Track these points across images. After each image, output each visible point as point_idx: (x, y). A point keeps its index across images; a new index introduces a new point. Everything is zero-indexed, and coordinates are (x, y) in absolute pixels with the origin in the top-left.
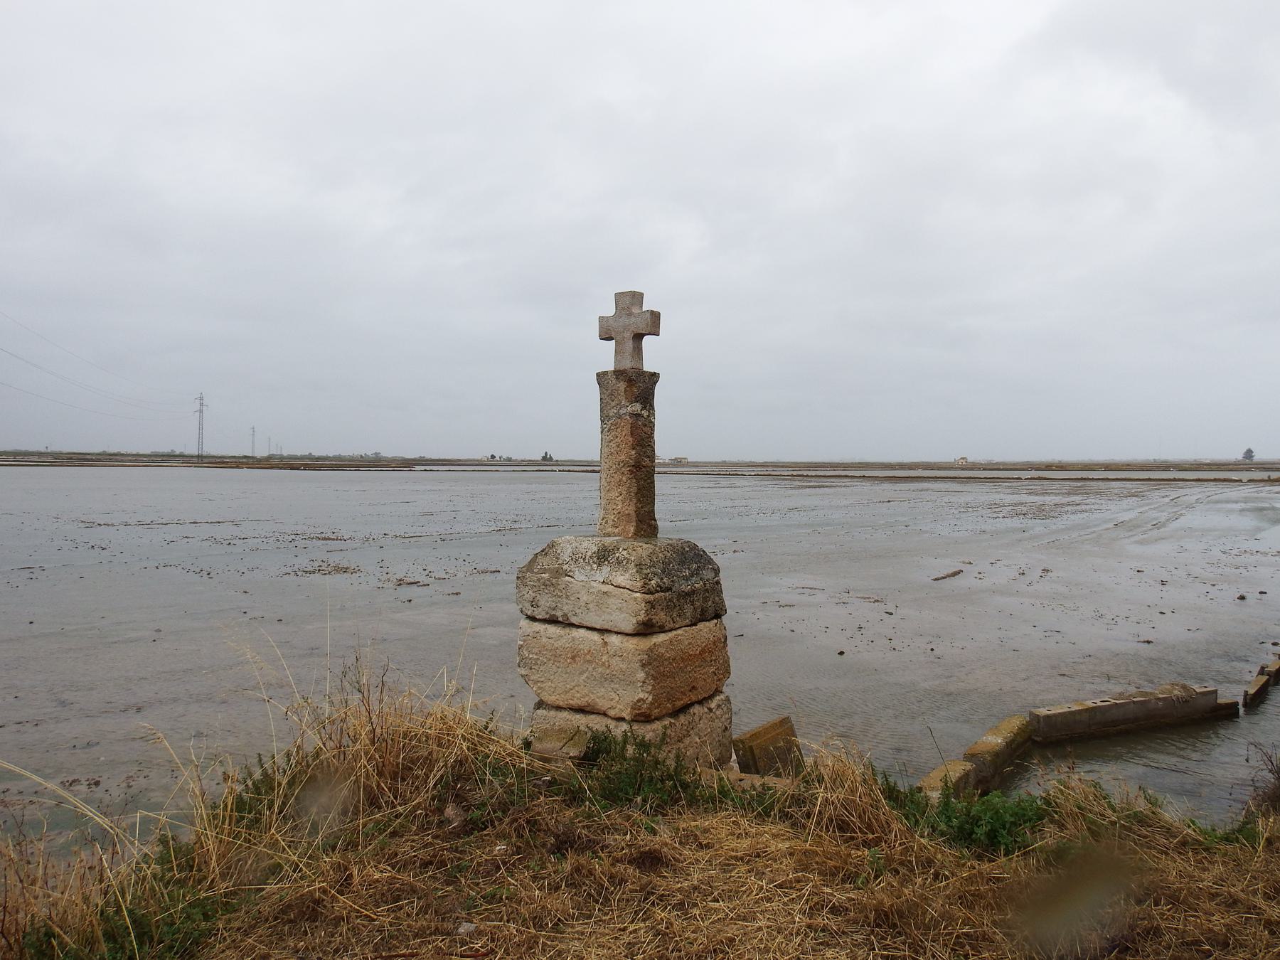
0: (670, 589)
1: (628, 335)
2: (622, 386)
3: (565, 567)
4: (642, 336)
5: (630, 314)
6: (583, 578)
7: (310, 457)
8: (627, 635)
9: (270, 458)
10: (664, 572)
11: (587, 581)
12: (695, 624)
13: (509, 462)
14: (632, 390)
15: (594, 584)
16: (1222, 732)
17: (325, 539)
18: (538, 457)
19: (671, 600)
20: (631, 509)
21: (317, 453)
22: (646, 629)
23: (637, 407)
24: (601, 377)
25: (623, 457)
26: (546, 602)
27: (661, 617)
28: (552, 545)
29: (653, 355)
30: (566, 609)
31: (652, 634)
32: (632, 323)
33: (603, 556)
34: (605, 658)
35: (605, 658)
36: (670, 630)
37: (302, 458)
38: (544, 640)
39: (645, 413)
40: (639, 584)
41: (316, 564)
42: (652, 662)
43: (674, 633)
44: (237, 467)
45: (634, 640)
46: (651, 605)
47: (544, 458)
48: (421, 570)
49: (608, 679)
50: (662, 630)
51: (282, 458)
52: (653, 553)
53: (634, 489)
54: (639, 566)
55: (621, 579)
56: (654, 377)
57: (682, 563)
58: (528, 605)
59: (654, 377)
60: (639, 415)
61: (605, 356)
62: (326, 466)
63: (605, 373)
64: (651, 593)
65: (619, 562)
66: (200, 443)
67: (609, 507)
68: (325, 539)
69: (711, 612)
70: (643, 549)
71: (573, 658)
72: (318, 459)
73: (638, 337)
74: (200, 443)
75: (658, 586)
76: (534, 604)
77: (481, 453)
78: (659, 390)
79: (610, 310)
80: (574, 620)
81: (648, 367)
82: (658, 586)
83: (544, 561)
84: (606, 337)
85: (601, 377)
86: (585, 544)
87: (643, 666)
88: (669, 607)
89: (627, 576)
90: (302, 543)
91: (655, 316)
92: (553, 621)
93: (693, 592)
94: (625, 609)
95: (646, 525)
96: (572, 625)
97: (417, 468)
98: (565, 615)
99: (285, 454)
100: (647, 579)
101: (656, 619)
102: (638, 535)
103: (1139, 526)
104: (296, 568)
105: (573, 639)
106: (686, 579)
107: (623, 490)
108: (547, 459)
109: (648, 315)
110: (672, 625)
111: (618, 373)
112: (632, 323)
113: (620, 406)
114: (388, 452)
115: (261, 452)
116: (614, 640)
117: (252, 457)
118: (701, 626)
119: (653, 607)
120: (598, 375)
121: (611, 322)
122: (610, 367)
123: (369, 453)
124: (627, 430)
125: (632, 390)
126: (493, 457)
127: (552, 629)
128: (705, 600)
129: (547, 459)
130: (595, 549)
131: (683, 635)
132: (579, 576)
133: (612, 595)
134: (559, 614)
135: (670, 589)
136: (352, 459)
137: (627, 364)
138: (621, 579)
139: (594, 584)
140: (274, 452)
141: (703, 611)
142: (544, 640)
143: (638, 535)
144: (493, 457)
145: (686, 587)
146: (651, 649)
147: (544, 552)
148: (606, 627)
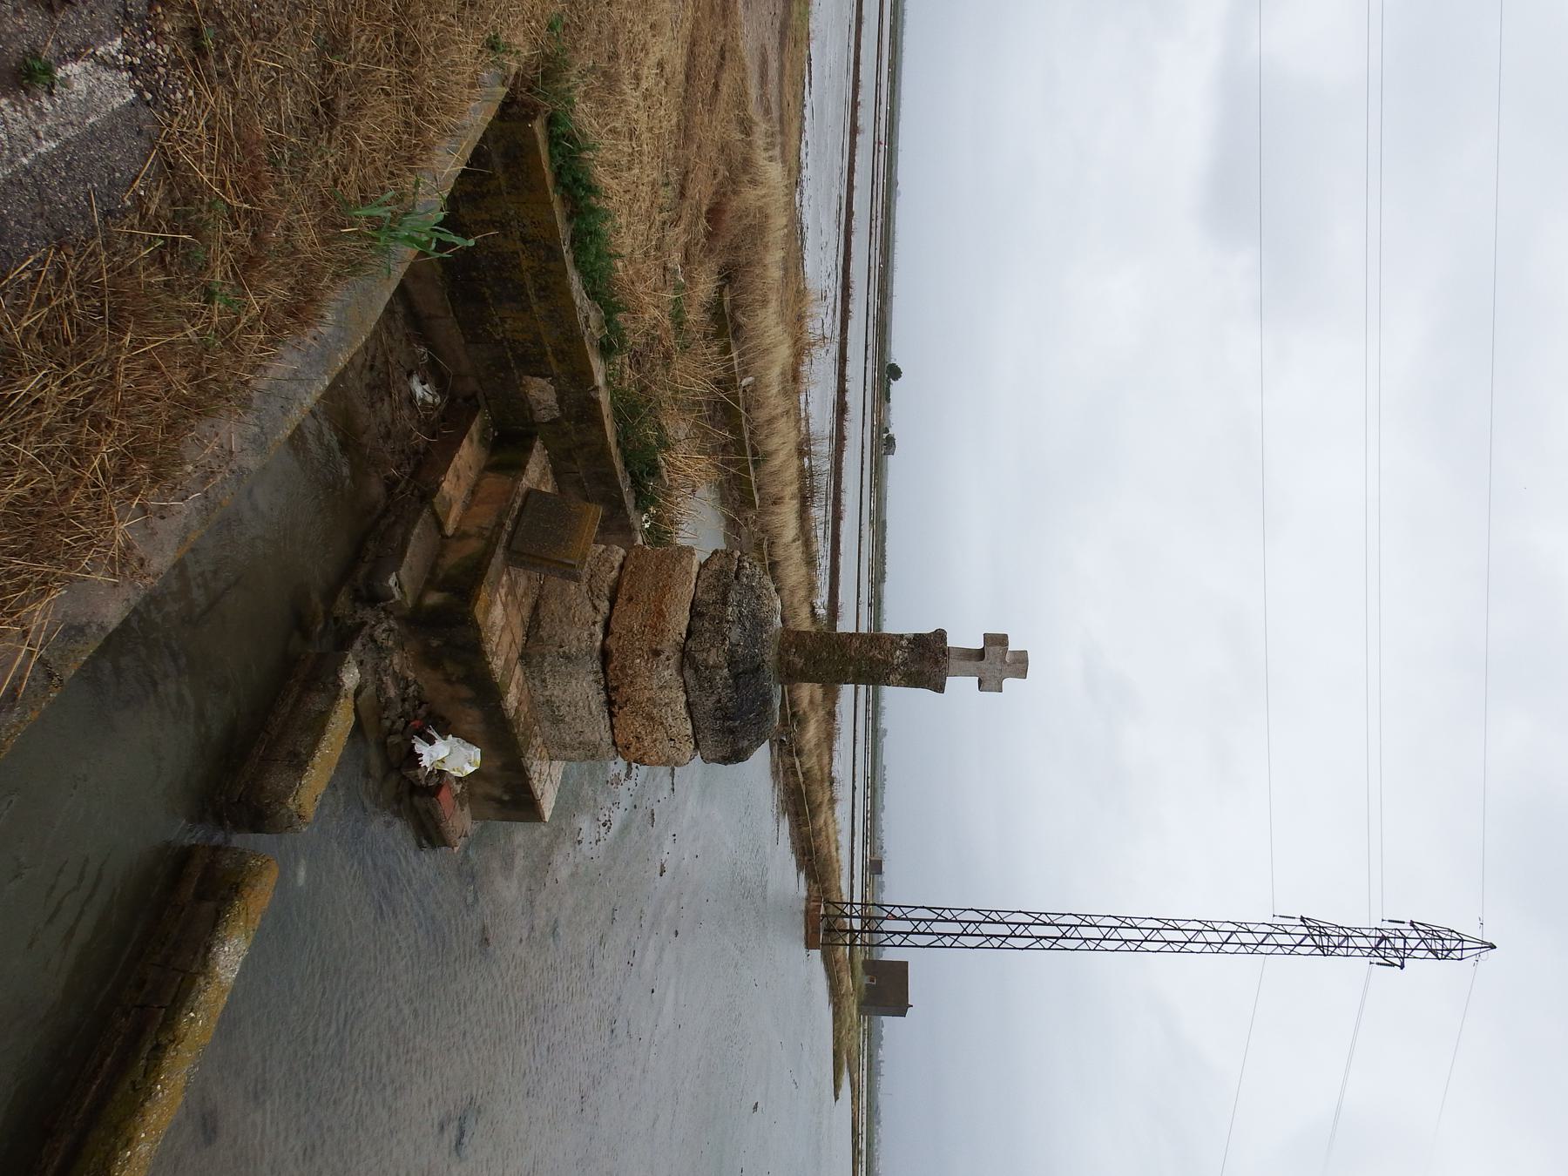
0: (737, 577)
14: (926, 660)
24: (941, 635)
29: (961, 686)
32: (997, 661)
39: (904, 643)
43: (694, 576)
56: (940, 688)
59: (940, 688)
77: (886, 722)
78: (925, 694)
79: (1008, 683)
81: (950, 682)
85: (941, 635)
93: (725, 603)
103: (782, 45)
106: (739, 605)
112: (997, 661)
114: (889, 589)
125: (926, 660)
131: (686, 591)
135: (737, 577)
141: (701, 615)
145: (732, 597)
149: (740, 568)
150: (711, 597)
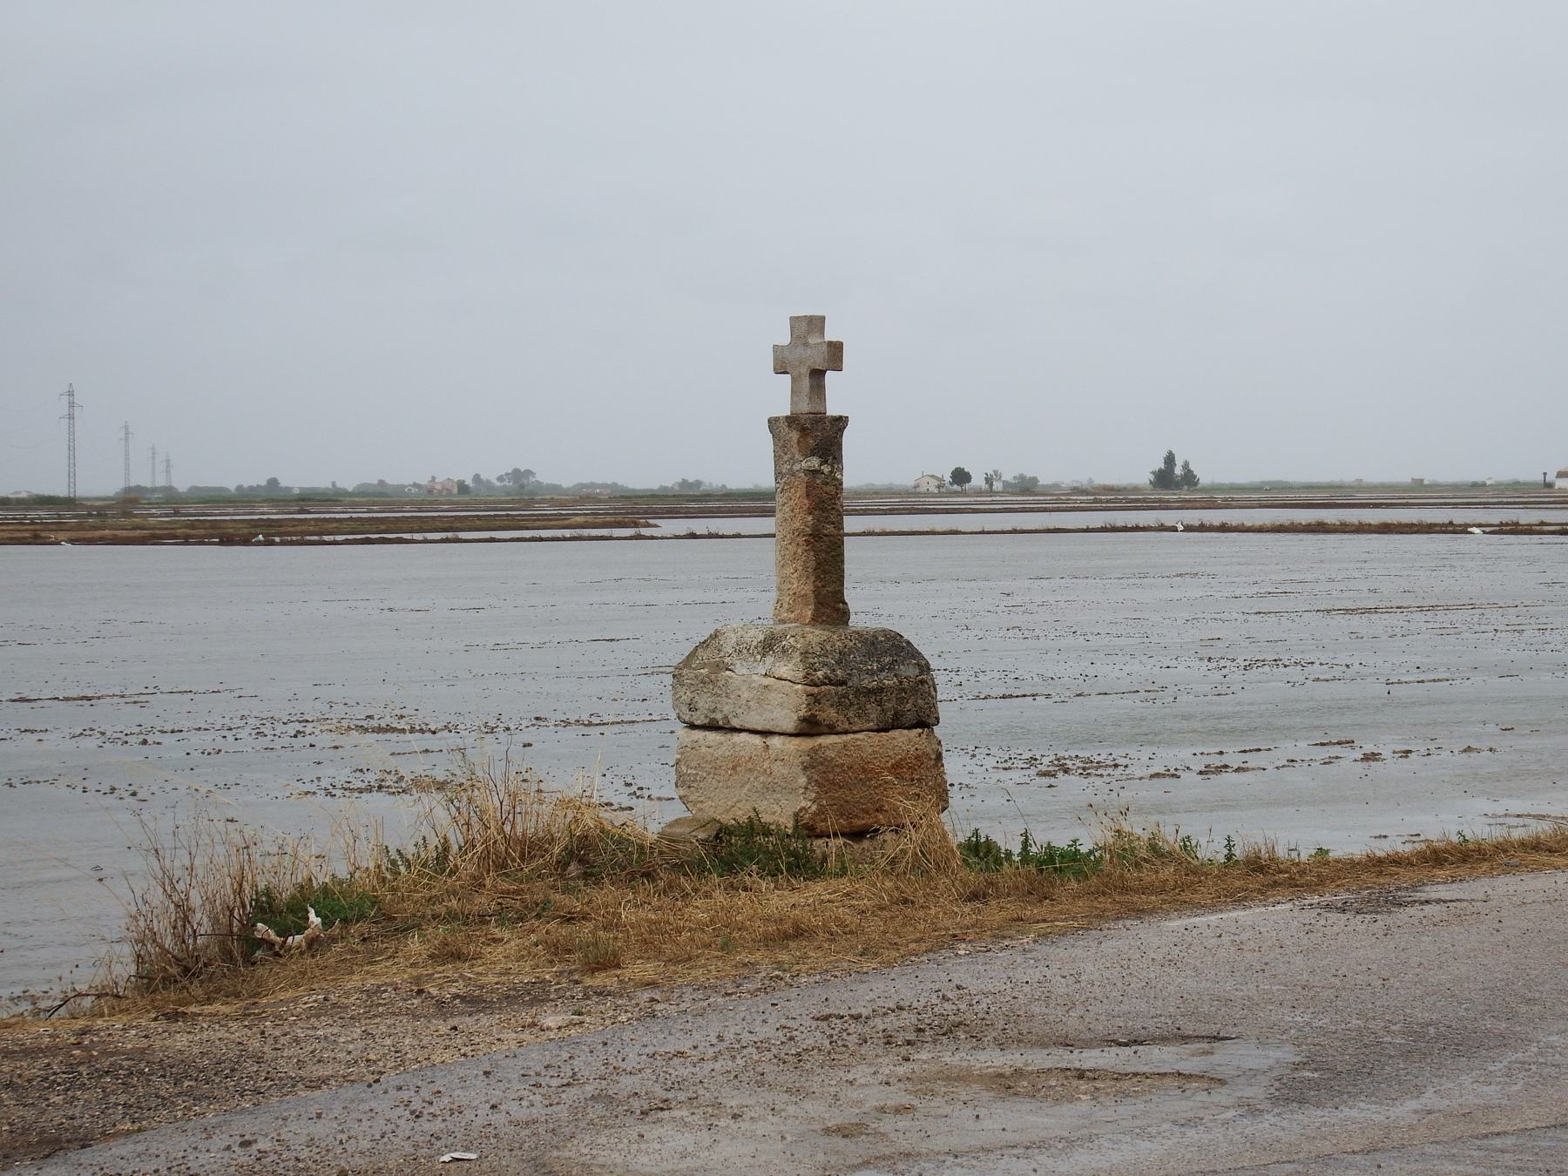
0: (843, 683)
1: (805, 371)
2: (795, 436)
3: (727, 660)
4: (822, 373)
5: (806, 344)
6: (744, 671)
7: (274, 494)
8: (791, 735)
9: (130, 501)
10: (839, 662)
11: (747, 674)
12: (886, 730)
13: (1027, 494)
14: (815, 436)
15: (755, 677)
16: (1455, 839)
17: (379, 730)
18: (1139, 474)
19: (845, 696)
20: (808, 589)
21: (299, 477)
22: (810, 727)
23: (814, 462)
24: (773, 422)
25: (797, 525)
26: (704, 702)
27: (829, 714)
28: (714, 636)
30: (726, 709)
31: (819, 734)
32: (812, 357)
33: (769, 645)
34: (766, 765)
35: (766, 765)
36: (846, 732)
37: (245, 498)
38: (704, 749)
39: (826, 469)
40: (801, 675)
41: (371, 778)
42: (813, 763)
43: (844, 738)
44: (36, 539)
45: (797, 741)
46: (815, 699)
47: (1164, 478)
48: (619, 784)
49: (769, 788)
50: (832, 730)
51: (172, 500)
52: (828, 640)
53: (812, 564)
54: (805, 654)
55: (784, 670)
56: (840, 422)
57: (870, 655)
58: (685, 709)
59: (840, 422)
60: (815, 473)
61: (780, 397)
62: (338, 527)
63: (777, 419)
64: (816, 685)
65: (784, 651)
66: (72, 475)
67: (784, 587)
68: (379, 730)
69: (910, 717)
70: (816, 635)
71: (734, 768)
72: (306, 500)
73: (817, 375)
74: (72, 475)
75: (826, 677)
76: (692, 708)
78: (850, 441)
79: (785, 338)
80: (735, 723)
81: (832, 410)
82: (826, 677)
83: (704, 655)
84: (780, 369)
85: (773, 422)
86: (751, 633)
87: (805, 769)
88: (841, 704)
89: (790, 666)
90: (325, 740)
91: (836, 350)
92: (712, 727)
93: (881, 690)
94: (785, 710)
95: (829, 604)
96: (734, 730)
97: (668, 526)
98: (726, 717)
99: (182, 484)
100: (812, 668)
101: (821, 716)
102: (816, 620)
104: (325, 783)
105: (734, 745)
106: (872, 673)
107: (799, 565)
108: (1172, 481)
109: (825, 348)
110: (847, 726)
111: (792, 420)
112: (812, 357)
113: (793, 461)
114: (564, 467)
115: (99, 481)
116: (776, 741)
117: (69, 503)
118: (895, 733)
119: (817, 701)
120: (770, 421)
121: (786, 353)
122: (786, 411)
123: (491, 474)
124: (801, 491)
126: (961, 476)
127: (712, 736)
128: (901, 701)
129: (1172, 481)
130: (762, 637)
131: (868, 743)
132: (741, 669)
133: (772, 692)
134: (719, 716)
135: (843, 683)
136: (428, 497)
137: (805, 407)
138: (784, 670)
139: (755, 677)
140: (143, 478)
141: (897, 715)
142: (704, 749)
143: (816, 620)
144: (961, 476)
145: (868, 682)
146: (814, 750)
147: (704, 644)
148: (768, 727)
149: (831, 682)
150: (873, 711)
